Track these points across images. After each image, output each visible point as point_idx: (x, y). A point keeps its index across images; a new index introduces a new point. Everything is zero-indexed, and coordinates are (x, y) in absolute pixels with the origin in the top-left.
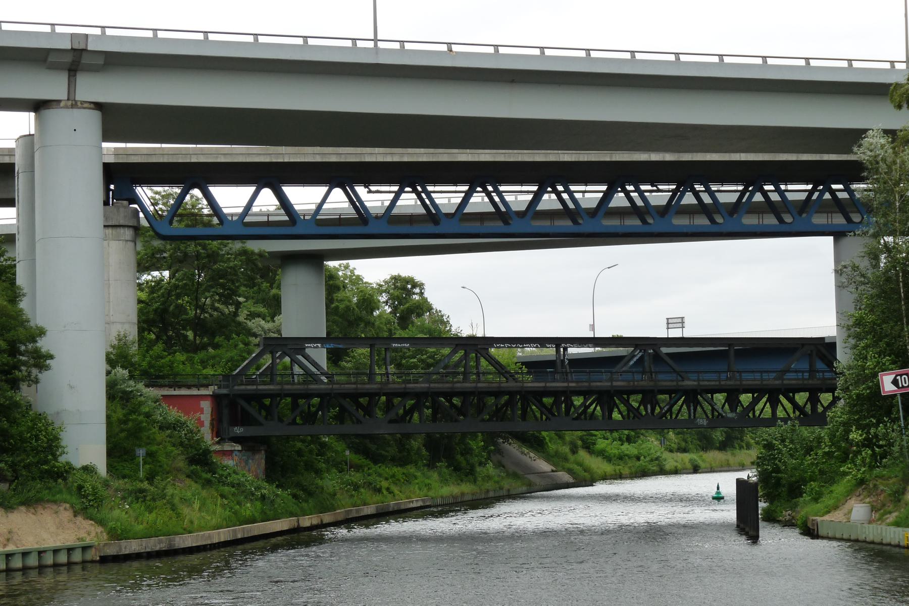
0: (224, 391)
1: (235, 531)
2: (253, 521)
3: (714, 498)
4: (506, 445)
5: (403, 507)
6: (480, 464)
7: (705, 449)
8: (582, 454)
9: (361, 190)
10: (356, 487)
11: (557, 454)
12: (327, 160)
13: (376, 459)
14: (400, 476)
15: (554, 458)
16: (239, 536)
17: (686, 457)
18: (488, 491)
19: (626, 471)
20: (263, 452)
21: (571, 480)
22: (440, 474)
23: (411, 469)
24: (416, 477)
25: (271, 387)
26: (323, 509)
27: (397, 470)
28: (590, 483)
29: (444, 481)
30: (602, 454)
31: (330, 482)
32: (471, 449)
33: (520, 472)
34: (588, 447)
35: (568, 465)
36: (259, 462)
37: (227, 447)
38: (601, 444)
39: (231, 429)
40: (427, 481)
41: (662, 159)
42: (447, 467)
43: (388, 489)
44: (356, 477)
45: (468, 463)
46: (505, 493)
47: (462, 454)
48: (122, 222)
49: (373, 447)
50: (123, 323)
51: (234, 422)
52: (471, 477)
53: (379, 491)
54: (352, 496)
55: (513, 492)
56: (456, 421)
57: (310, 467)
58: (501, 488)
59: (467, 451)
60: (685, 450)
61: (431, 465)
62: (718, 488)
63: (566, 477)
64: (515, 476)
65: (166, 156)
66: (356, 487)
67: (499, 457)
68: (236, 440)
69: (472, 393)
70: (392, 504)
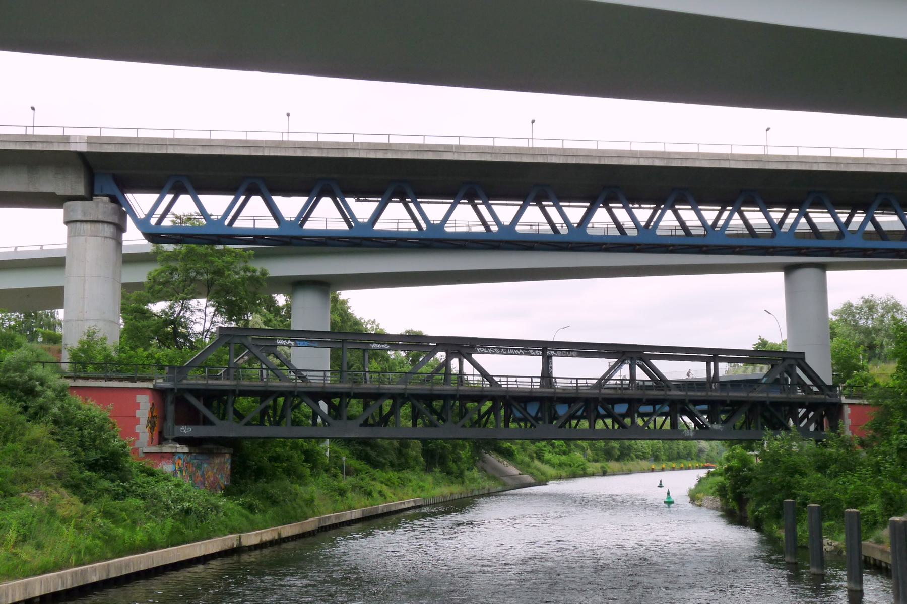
0: (169, 385)
1: (83, 573)
2: (151, 546)
3: (665, 502)
4: (487, 455)
5: (393, 509)
6: (468, 469)
7: (607, 460)
8: (537, 463)
9: (350, 201)
10: (342, 493)
11: (522, 462)
12: (309, 155)
13: (376, 465)
14: (395, 480)
15: (524, 467)
16: (113, 575)
17: (598, 465)
18: (473, 491)
19: (564, 474)
20: (227, 456)
21: (533, 481)
22: (434, 478)
23: (407, 474)
24: (410, 481)
25: (227, 382)
26: (288, 519)
27: (392, 475)
28: (544, 483)
29: (437, 483)
30: (548, 462)
31: (313, 489)
32: (461, 458)
33: (497, 475)
34: (540, 457)
35: (530, 470)
36: (219, 468)
37: (167, 449)
38: (547, 456)
39: (176, 427)
40: (421, 484)
41: (651, 164)
42: (441, 472)
43: (380, 492)
44: (346, 482)
45: (459, 468)
46: (486, 491)
47: (454, 461)
48: (101, 218)
49: (373, 454)
50: (97, 320)
51: (179, 422)
52: (460, 479)
53: (369, 494)
54: (336, 501)
55: (493, 490)
56: (436, 426)
57: (293, 473)
58: (483, 488)
59: (457, 460)
60: (596, 461)
61: (428, 469)
62: (668, 494)
63: (528, 478)
64: (495, 478)
65: (141, 147)
66: (342, 493)
67: (361, 421)
68: (181, 441)
69: (453, 397)
70: (382, 507)
